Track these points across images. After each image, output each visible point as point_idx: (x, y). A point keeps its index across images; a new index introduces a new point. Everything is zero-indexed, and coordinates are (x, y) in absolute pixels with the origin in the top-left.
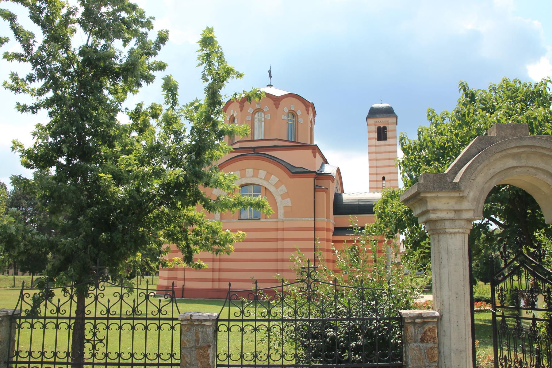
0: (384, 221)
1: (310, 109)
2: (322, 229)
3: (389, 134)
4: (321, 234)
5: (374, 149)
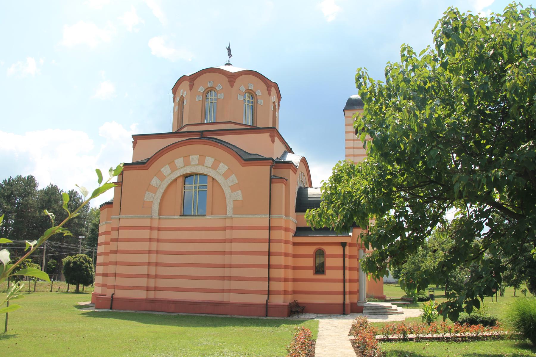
0: (334, 207)
1: (273, 90)
2: (279, 228)
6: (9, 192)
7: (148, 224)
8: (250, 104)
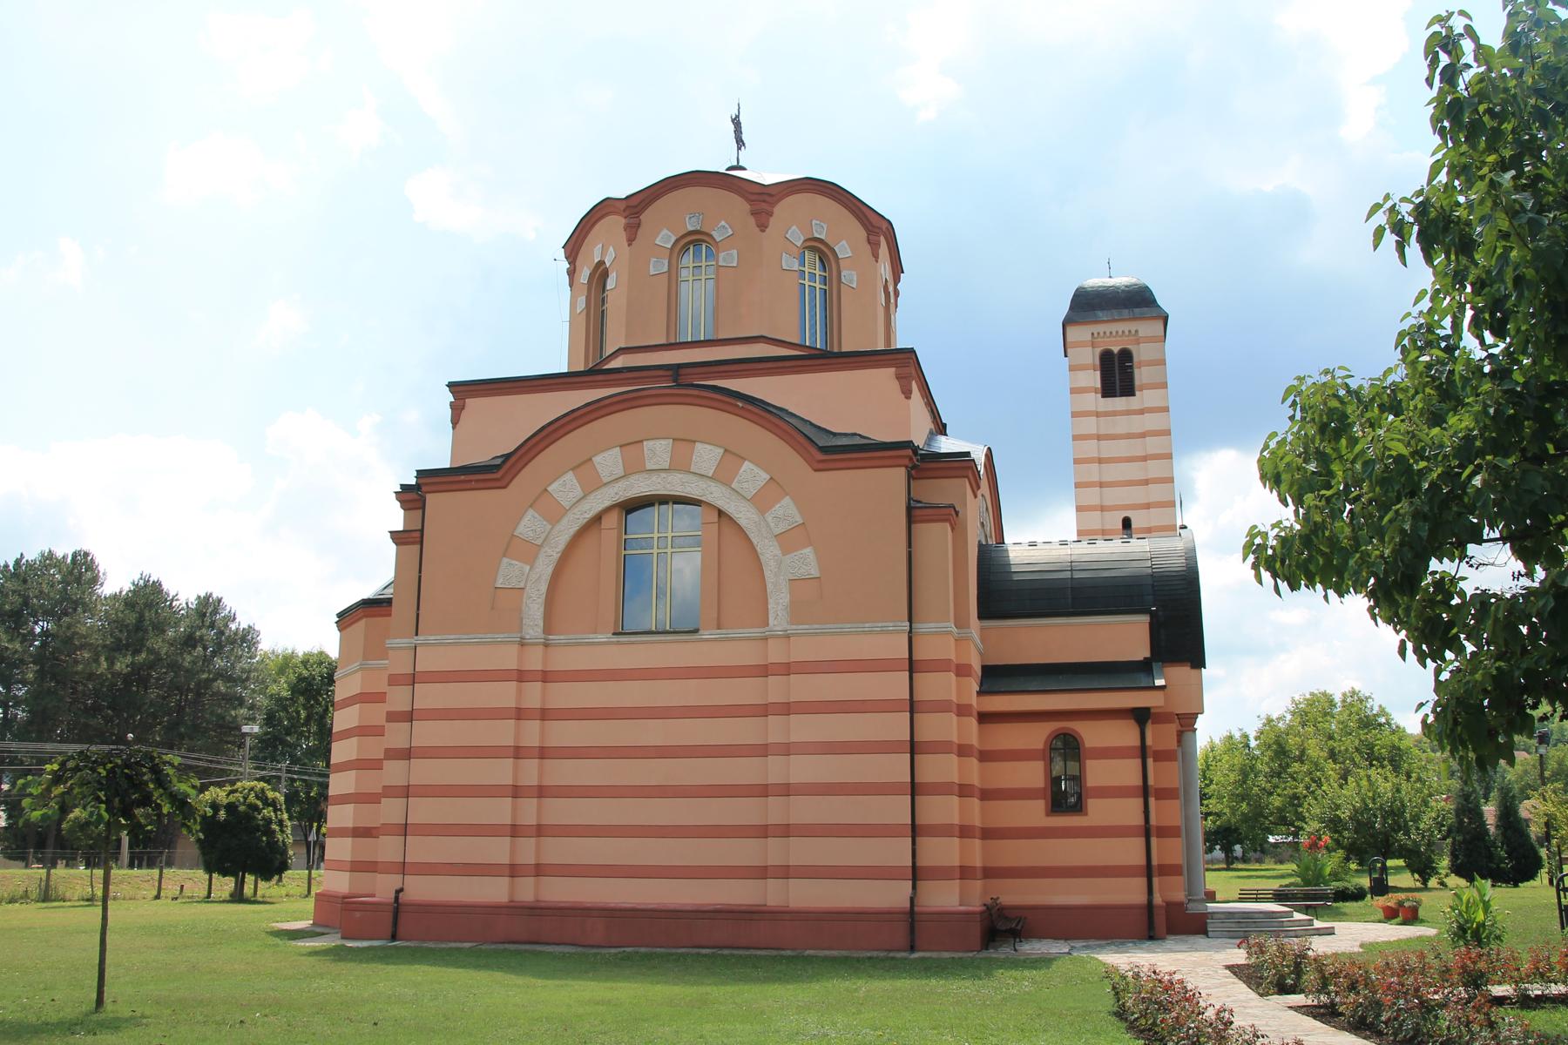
3: (1141, 375)
4: (935, 686)
5: (1090, 425)
6: (17, 599)
7: (508, 658)
8: (818, 285)
